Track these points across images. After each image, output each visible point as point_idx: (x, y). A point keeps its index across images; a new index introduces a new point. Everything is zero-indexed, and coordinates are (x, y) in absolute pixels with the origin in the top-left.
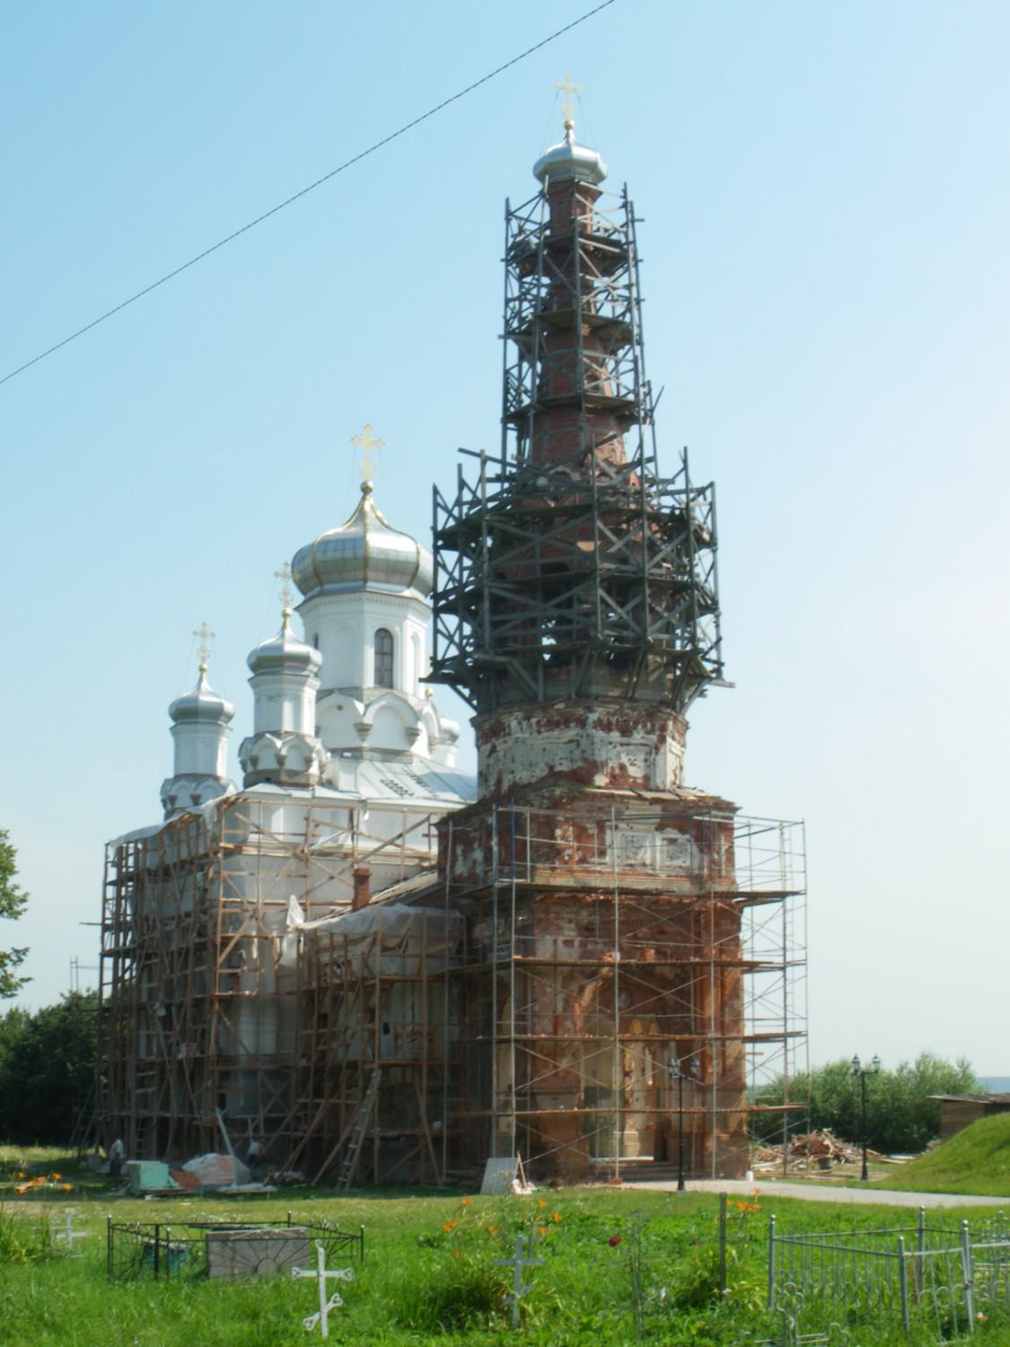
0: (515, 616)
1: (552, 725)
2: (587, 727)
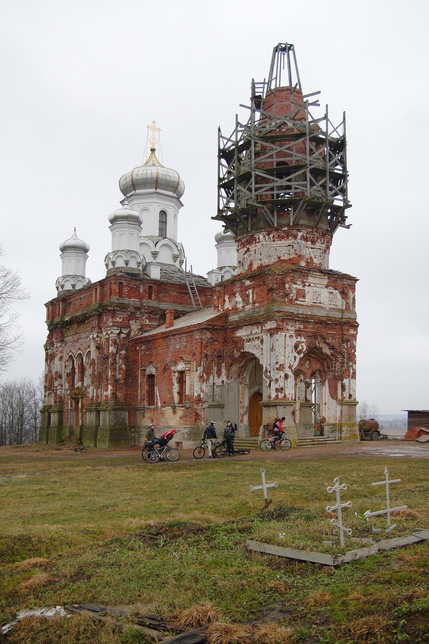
0: (268, 185)
1: (281, 238)
2: (297, 239)
